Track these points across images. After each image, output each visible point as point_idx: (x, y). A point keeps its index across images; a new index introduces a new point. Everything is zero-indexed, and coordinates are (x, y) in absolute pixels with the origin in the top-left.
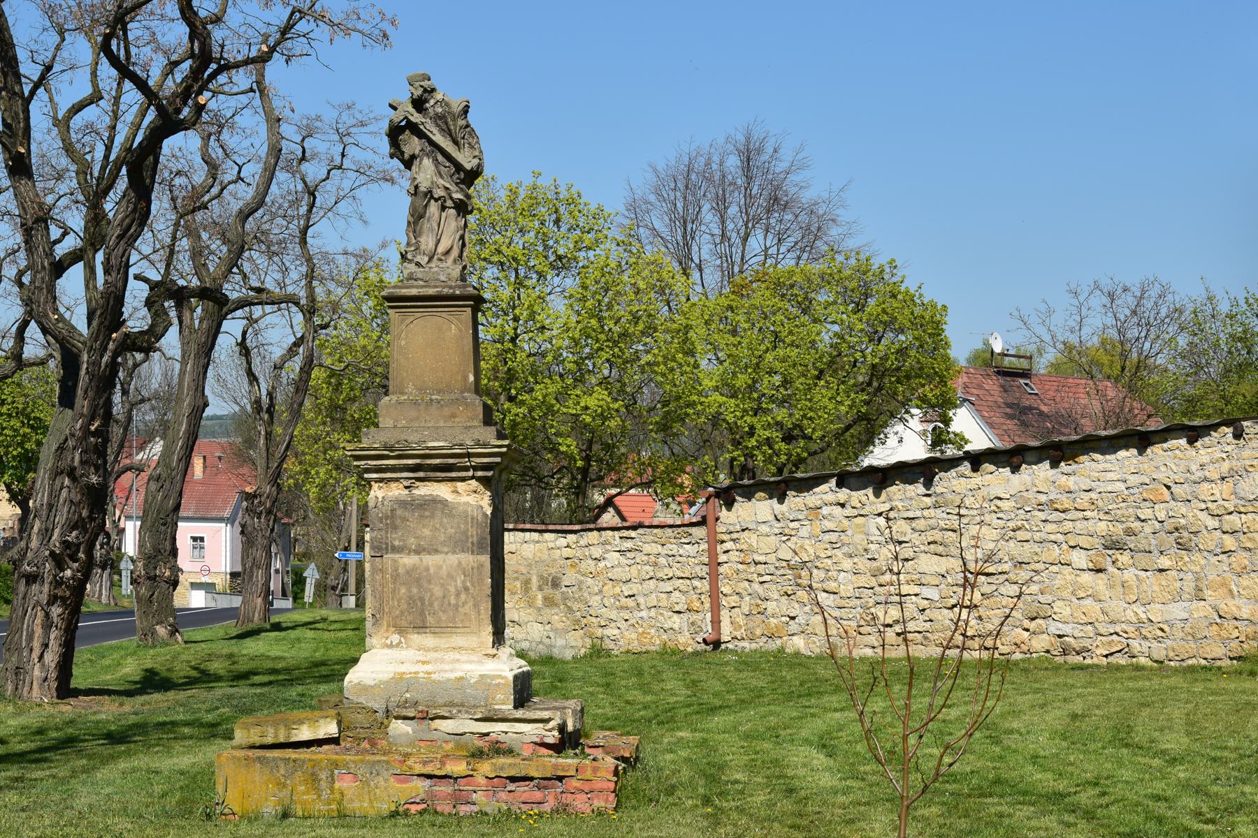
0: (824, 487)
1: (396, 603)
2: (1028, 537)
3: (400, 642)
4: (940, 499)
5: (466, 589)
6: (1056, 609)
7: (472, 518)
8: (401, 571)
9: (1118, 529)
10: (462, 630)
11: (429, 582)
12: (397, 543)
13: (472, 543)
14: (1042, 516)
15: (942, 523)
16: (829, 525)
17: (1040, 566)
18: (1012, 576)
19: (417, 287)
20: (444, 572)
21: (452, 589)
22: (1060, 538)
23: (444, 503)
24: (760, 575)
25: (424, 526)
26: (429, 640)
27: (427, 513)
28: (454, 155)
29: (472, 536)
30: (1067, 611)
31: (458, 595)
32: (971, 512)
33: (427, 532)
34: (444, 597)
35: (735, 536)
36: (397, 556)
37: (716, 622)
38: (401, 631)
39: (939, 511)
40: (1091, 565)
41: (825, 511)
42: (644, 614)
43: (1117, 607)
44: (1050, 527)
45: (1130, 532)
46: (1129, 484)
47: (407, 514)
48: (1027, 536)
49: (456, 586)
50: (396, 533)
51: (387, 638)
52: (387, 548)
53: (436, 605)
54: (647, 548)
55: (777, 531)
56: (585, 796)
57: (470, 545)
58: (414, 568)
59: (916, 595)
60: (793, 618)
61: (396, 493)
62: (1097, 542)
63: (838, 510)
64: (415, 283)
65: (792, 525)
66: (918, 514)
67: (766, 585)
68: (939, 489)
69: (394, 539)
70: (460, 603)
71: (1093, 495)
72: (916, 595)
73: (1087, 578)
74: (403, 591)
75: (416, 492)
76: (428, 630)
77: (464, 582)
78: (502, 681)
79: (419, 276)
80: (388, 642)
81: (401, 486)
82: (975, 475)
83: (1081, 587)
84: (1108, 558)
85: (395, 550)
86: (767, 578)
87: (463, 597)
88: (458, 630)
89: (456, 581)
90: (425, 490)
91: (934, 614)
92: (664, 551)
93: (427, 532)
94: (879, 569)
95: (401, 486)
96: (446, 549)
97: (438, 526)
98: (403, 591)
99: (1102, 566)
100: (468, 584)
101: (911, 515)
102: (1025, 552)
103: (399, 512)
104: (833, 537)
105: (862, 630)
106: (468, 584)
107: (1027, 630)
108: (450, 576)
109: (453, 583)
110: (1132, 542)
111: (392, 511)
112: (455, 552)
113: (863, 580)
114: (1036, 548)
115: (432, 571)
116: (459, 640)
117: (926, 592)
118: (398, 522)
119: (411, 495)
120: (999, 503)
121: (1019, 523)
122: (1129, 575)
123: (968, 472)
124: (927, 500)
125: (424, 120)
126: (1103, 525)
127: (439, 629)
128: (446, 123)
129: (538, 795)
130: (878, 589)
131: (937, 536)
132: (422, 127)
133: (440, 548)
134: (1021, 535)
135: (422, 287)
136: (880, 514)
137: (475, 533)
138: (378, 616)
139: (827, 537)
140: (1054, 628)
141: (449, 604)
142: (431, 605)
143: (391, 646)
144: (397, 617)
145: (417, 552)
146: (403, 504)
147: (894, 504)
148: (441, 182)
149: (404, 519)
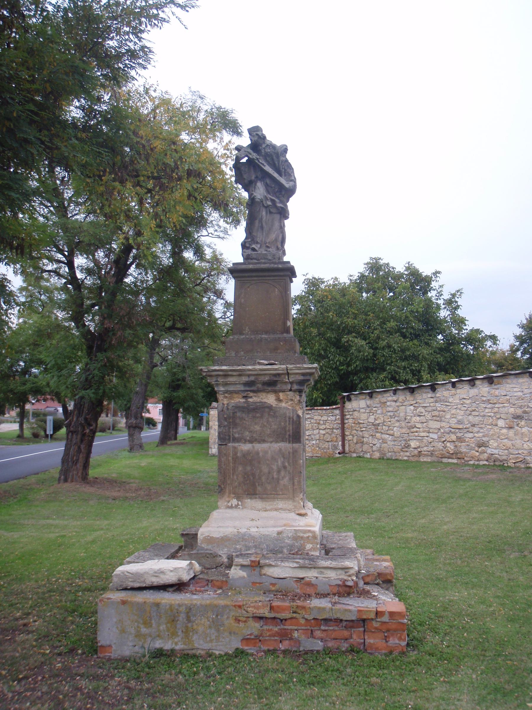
0: (388, 395)
1: (235, 477)
2: (477, 414)
3: (238, 505)
4: (438, 399)
5: (285, 467)
6: (491, 443)
7: (289, 418)
8: (239, 454)
9: (519, 412)
10: (282, 496)
11: (259, 462)
12: (237, 435)
13: (289, 435)
14: (484, 406)
15: (438, 408)
16: (391, 409)
17: (483, 426)
18: (470, 430)
19: (253, 264)
20: (269, 455)
21: (275, 467)
22: (493, 414)
23: (270, 407)
24: (361, 428)
25: (256, 424)
26: (258, 504)
27: (258, 415)
28: (278, 179)
29: (289, 431)
30: (495, 444)
31: (279, 472)
32: (452, 404)
33: (257, 428)
34: (269, 473)
35: (351, 413)
36: (236, 445)
37: (343, 446)
38: (238, 498)
39: (437, 404)
40: (507, 426)
41: (388, 404)
42: (314, 442)
43: (518, 442)
44: (487, 410)
45: (525, 412)
46: (525, 393)
47: (244, 415)
48: (477, 414)
49: (278, 465)
50: (236, 428)
51: (229, 502)
52: (229, 439)
53: (263, 479)
54: (316, 417)
55: (368, 411)
56: (383, 634)
57: (287, 437)
58: (249, 453)
59: (427, 437)
60: (375, 445)
61: (237, 400)
62: (510, 417)
63: (393, 404)
64: (252, 261)
65: (374, 409)
66: (428, 405)
67: (363, 432)
68: (438, 395)
69: (235, 433)
70: (281, 477)
71: (508, 397)
72: (427, 437)
73: (504, 431)
74: (240, 469)
75: (250, 400)
76: (257, 496)
77: (283, 463)
78: (310, 534)
79: (254, 256)
80: (230, 504)
81: (240, 396)
82: (453, 389)
83: (503, 434)
84: (515, 423)
85: (235, 440)
86: (364, 429)
87: (283, 473)
88: (279, 496)
89: (277, 462)
90: (254, 399)
91: (436, 444)
92: (322, 419)
93: (257, 428)
94: (411, 426)
95: (240, 396)
96: (271, 440)
97: (265, 424)
98: (240, 469)
99: (512, 426)
100: (287, 464)
101: (425, 405)
102: (476, 420)
103: (238, 414)
104: (392, 414)
105: (403, 450)
106: (287, 464)
107: (478, 451)
108: (274, 459)
109: (276, 463)
110: (526, 416)
111: (233, 413)
112: (277, 442)
113: (404, 431)
114: (481, 418)
115: (261, 454)
116: (281, 504)
117: (431, 435)
118: (238, 421)
119: (247, 402)
120: (464, 401)
121: (474, 408)
122: (525, 430)
123: (451, 388)
124: (432, 399)
125: (258, 157)
126: (512, 409)
127: (264, 496)
128: (273, 159)
129: (346, 633)
130: (410, 434)
131: (436, 413)
132: (257, 161)
133: (266, 439)
134: (473, 413)
135: (256, 263)
136: (412, 405)
137: (291, 428)
138: (223, 486)
139: (389, 414)
140: (489, 451)
141: (273, 478)
142: (260, 478)
143: (231, 507)
144: (236, 487)
145: (251, 442)
146: (238, 408)
147: (418, 401)
148: (269, 196)
149: (242, 419)
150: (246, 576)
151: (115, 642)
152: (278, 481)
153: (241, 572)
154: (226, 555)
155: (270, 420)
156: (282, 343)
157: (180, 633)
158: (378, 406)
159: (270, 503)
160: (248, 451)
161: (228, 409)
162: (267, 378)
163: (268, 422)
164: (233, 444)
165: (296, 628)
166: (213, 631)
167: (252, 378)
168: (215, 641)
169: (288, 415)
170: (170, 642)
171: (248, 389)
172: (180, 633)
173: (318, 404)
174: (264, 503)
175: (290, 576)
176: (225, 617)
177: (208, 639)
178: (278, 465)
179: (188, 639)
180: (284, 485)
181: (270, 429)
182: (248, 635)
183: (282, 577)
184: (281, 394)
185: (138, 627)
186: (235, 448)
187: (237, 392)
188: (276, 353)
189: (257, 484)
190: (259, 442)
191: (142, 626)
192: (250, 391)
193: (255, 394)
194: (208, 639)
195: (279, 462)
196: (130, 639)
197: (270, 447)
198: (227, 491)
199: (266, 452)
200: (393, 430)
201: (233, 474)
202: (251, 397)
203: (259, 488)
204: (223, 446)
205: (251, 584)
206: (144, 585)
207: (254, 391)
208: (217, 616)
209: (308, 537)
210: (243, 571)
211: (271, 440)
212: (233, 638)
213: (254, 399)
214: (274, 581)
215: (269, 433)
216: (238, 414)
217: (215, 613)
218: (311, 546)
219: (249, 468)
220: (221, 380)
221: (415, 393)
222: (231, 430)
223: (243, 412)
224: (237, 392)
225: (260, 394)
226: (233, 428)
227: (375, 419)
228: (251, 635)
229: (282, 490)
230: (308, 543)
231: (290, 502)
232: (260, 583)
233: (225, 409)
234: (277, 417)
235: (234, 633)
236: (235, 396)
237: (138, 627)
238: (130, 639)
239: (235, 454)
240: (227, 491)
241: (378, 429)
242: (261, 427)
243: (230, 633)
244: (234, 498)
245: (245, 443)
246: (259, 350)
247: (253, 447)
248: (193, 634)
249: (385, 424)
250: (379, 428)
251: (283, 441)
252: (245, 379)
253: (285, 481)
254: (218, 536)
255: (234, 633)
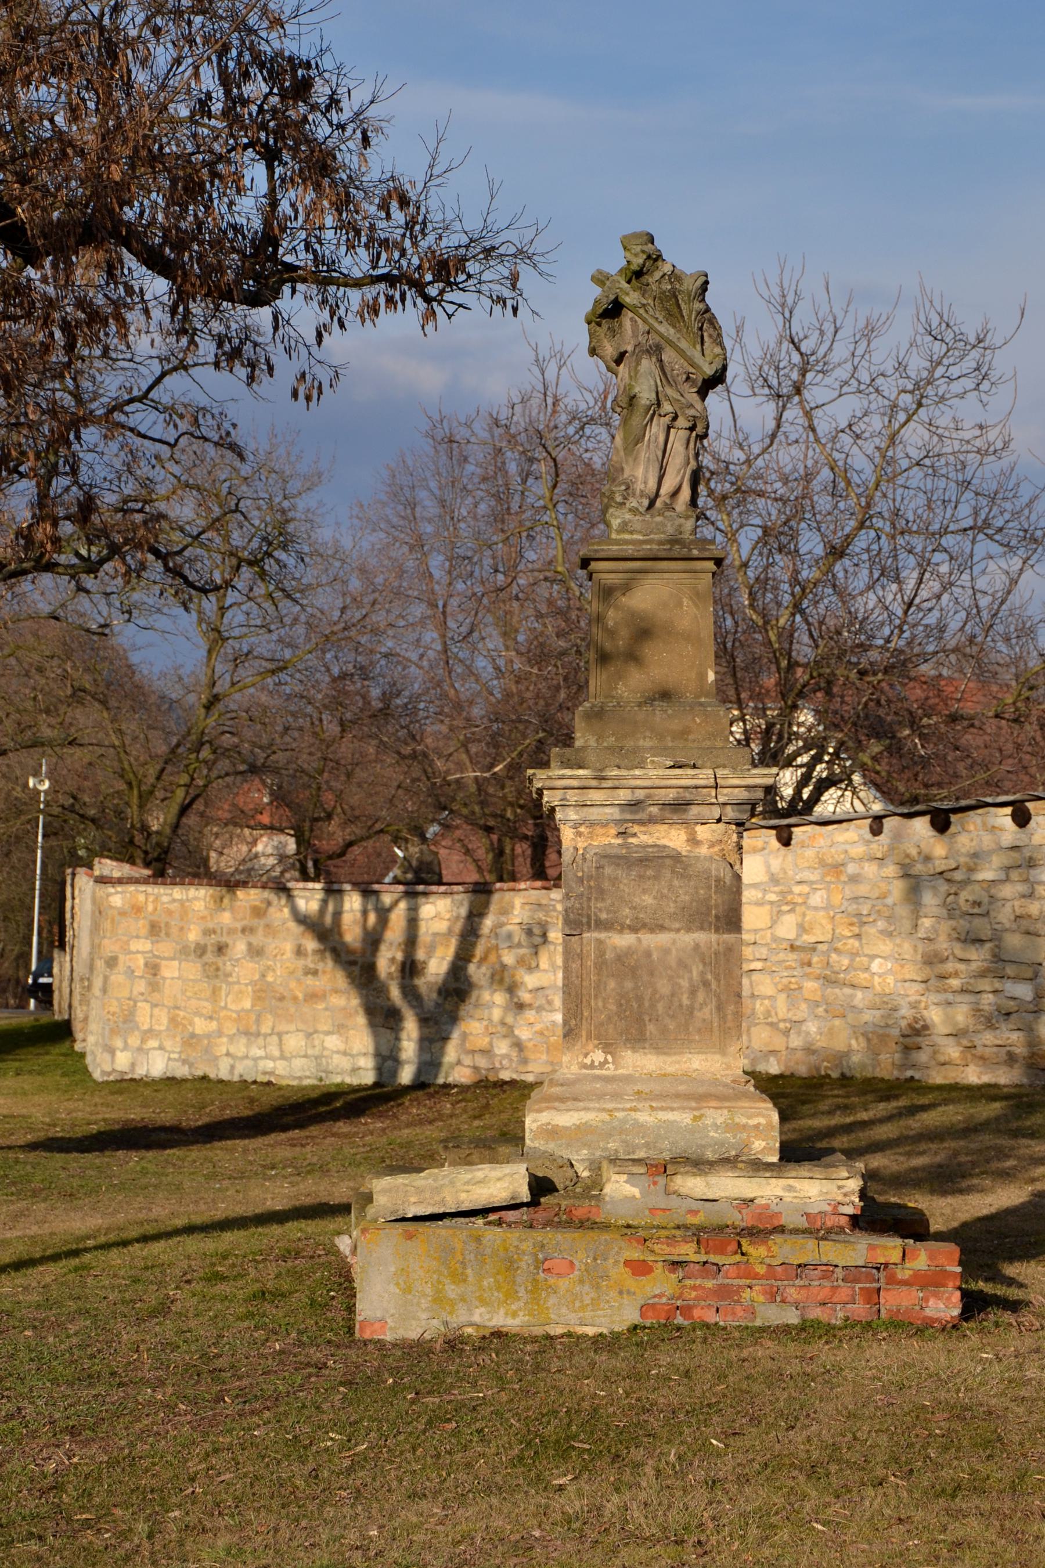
1: (600, 1004)
3: (606, 1062)
5: (706, 984)
11: (651, 974)
12: (604, 916)
21: (685, 983)
23: (676, 857)
25: (644, 891)
27: (650, 873)
29: (717, 906)
31: (693, 992)
33: (648, 900)
34: (673, 995)
36: (602, 936)
38: (607, 1047)
49: (691, 979)
51: (586, 1055)
53: (660, 1007)
58: (629, 952)
65: (797, 889)
69: (600, 910)
70: (697, 1006)
74: (612, 984)
75: (631, 840)
80: (588, 1061)
86: (758, 965)
87: (701, 996)
89: (691, 972)
90: (644, 837)
93: (648, 900)
96: (677, 925)
97: (665, 891)
103: (608, 870)
106: (709, 977)
108: (682, 964)
112: (689, 930)
115: (655, 956)
118: (606, 885)
133: (667, 923)
141: (681, 1006)
144: (602, 1024)
145: (634, 929)
146: (607, 857)
150: (638, 1195)
151: (392, 1311)
152: (692, 1013)
153: (628, 1187)
154: (587, 1164)
155: (676, 883)
156: (698, 720)
157: (522, 1293)
158: (814, 876)
159: (674, 1058)
160: (629, 948)
161: (584, 859)
162: (671, 795)
163: (670, 887)
164: (595, 935)
165: (748, 1282)
166: (587, 1288)
167: (640, 794)
168: (590, 1308)
169: (714, 873)
170: (502, 1311)
171: (629, 817)
172: (522, 1293)
173: (26, 949)
174: (662, 1058)
175: (727, 1194)
176: (611, 1261)
177: (577, 1304)
178: (691, 979)
179: (538, 1304)
180: (704, 1020)
181: (676, 902)
182: (655, 1296)
183: (711, 1197)
184: (699, 828)
185: (439, 1282)
186: (600, 942)
187: (605, 824)
188: (686, 740)
189: (647, 1018)
190: (652, 931)
191: (447, 1281)
192: (633, 821)
193: (643, 829)
194: (577, 1304)
195: (695, 973)
196: (423, 1306)
197: (674, 942)
198: (584, 1033)
199: (667, 951)
200: (867, 969)
201: (596, 996)
202: (635, 835)
203: (651, 1028)
204: (573, 939)
205: (647, 1212)
206: (441, 1211)
207: (641, 823)
208: (595, 1259)
209: (757, 1127)
210: (633, 1185)
211: (677, 925)
212: (626, 1302)
213: (644, 837)
214: (695, 1205)
215: (672, 910)
216: (608, 870)
217: (591, 1254)
218: (763, 1144)
219: (629, 985)
220: (573, 796)
221: (953, 829)
222: (592, 904)
223: (618, 865)
224: (605, 824)
225: (652, 828)
226: (596, 899)
227: (802, 928)
228: (660, 1296)
229: (699, 1031)
230: (757, 1137)
231: (717, 1057)
232: (664, 1210)
233: (579, 859)
234: (689, 877)
235: (628, 1292)
236: (600, 830)
237: (439, 1282)
238: (423, 1306)
239: (601, 953)
240: (584, 1033)
241: (809, 964)
242: (655, 898)
243: (621, 1293)
244: (596, 1047)
245: (621, 932)
246: (648, 734)
247: (639, 940)
248: (548, 1296)
249: (839, 945)
250: (815, 959)
251: (702, 928)
252: (624, 795)
253: (707, 1013)
254: (568, 1124)
255: (628, 1292)
